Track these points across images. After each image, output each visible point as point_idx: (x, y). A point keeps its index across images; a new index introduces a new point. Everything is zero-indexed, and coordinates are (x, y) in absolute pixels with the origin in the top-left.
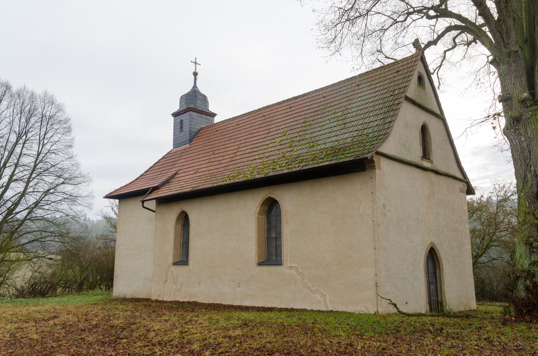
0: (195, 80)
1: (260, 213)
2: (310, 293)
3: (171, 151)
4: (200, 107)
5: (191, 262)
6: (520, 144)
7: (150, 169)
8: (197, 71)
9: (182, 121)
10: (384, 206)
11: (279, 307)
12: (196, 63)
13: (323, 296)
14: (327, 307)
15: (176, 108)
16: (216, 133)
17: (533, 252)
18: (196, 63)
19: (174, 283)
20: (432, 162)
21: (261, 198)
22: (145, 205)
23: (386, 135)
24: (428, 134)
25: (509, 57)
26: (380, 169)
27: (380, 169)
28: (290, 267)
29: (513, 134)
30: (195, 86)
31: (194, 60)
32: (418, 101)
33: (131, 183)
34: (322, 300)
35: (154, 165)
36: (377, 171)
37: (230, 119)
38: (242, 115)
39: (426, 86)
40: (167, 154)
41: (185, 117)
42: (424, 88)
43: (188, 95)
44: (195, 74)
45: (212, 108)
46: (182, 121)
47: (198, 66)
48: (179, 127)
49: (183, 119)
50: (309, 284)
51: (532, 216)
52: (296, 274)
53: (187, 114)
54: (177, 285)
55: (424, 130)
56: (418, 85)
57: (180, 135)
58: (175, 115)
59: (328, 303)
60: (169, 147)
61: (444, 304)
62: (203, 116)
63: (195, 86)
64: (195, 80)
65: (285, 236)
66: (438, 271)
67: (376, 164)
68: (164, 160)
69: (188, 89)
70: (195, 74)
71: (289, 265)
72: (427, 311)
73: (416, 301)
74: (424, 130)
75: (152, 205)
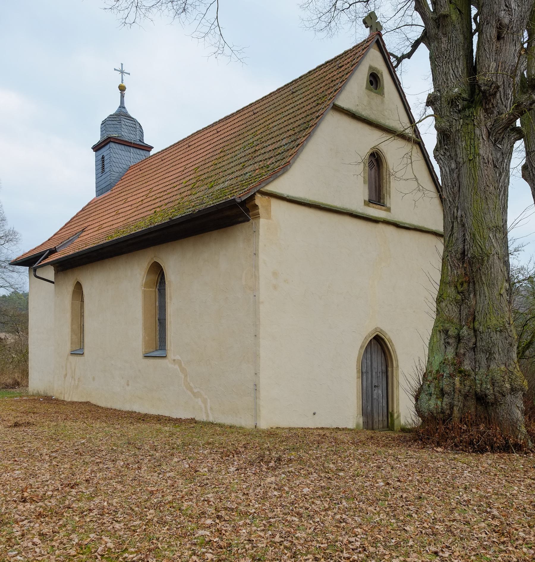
0: (122, 96)
1: (146, 285)
2: (192, 396)
3: (94, 199)
4: (126, 135)
5: (86, 351)
6: (450, 174)
7: (66, 225)
8: (124, 84)
9: (103, 157)
10: (275, 274)
11: (175, 415)
12: (122, 72)
13: (205, 401)
14: (208, 416)
15: (97, 139)
16: (140, 172)
17: (448, 343)
18: (122, 72)
19: (72, 377)
20: (389, 210)
21: (147, 264)
22: (37, 275)
23: (285, 168)
24: (385, 166)
25: (438, 27)
26: (269, 217)
27: (269, 217)
28: (174, 360)
29: (442, 157)
30: (122, 106)
31: (119, 67)
32: (365, 113)
33: (42, 245)
34: (203, 406)
35: (71, 220)
36: (262, 221)
37: (159, 152)
38: (170, 147)
39: (386, 90)
40: (88, 205)
41: (104, 151)
42: (382, 94)
43: (111, 118)
44: (122, 89)
45: (147, 141)
46: (103, 157)
47: (126, 76)
48: (102, 166)
49: (105, 154)
50: (192, 385)
51: (453, 289)
52: (179, 370)
53: (107, 147)
54: (75, 380)
55: (376, 160)
56: (367, 88)
57: (103, 177)
58: (97, 148)
59: (209, 411)
60: (91, 195)
61: (396, 415)
62: (132, 149)
63: (122, 106)
64: (122, 96)
65: (169, 317)
66: (390, 369)
67: (261, 211)
68: (83, 212)
69: (113, 109)
70: (122, 89)
71: (173, 358)
72: (358, 425)
73: (346, 412)
74: (376, 160)
75: (50, 273)
